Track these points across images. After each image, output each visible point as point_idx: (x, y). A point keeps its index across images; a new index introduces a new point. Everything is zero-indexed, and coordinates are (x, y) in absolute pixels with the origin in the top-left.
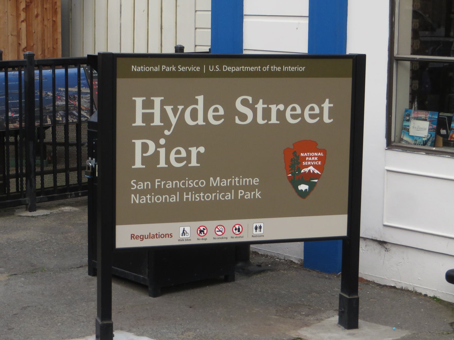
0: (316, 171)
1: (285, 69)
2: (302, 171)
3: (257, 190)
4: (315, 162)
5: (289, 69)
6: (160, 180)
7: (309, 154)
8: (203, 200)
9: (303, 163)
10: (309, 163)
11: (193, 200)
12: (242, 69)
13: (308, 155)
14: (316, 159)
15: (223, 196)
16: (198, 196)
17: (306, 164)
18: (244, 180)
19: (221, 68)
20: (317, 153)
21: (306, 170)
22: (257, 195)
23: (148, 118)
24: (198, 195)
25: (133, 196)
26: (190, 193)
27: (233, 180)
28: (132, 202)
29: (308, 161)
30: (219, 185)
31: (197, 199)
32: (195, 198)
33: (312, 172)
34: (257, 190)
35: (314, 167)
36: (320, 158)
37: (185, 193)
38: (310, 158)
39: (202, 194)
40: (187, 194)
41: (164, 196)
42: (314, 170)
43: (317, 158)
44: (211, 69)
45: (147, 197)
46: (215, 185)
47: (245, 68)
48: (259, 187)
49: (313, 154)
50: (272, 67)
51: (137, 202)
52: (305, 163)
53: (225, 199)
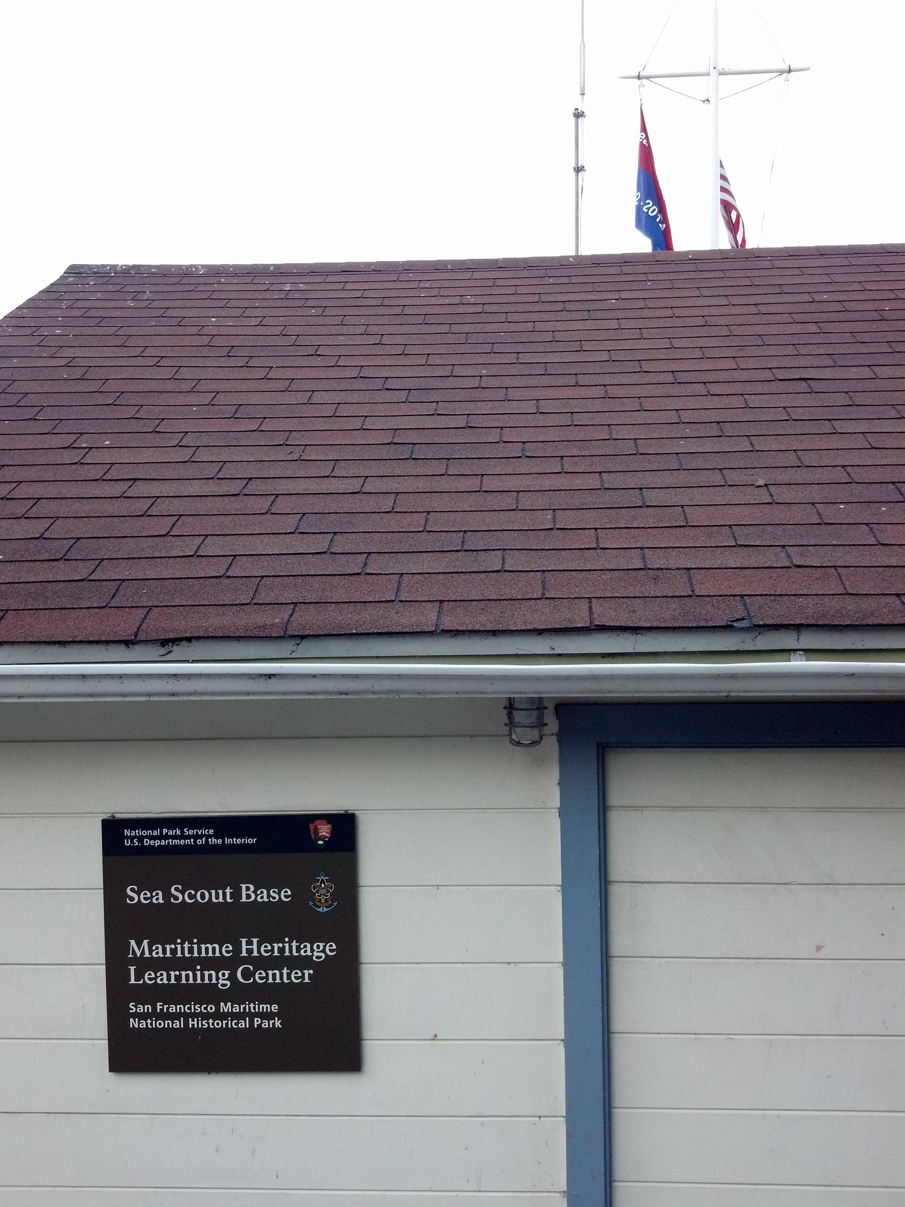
6: (161, 1004)
11: (200, 1027)
12: (169, 842)
18: (261, 1006)
23: (250, 951)
25: (131, 1020)
27: (247, 1006)
30: (230, 1011)
39: (211, 1021)
44: (128, 843)
46: (226, 1011)
48: (278, 1015)
50: (210, 840)
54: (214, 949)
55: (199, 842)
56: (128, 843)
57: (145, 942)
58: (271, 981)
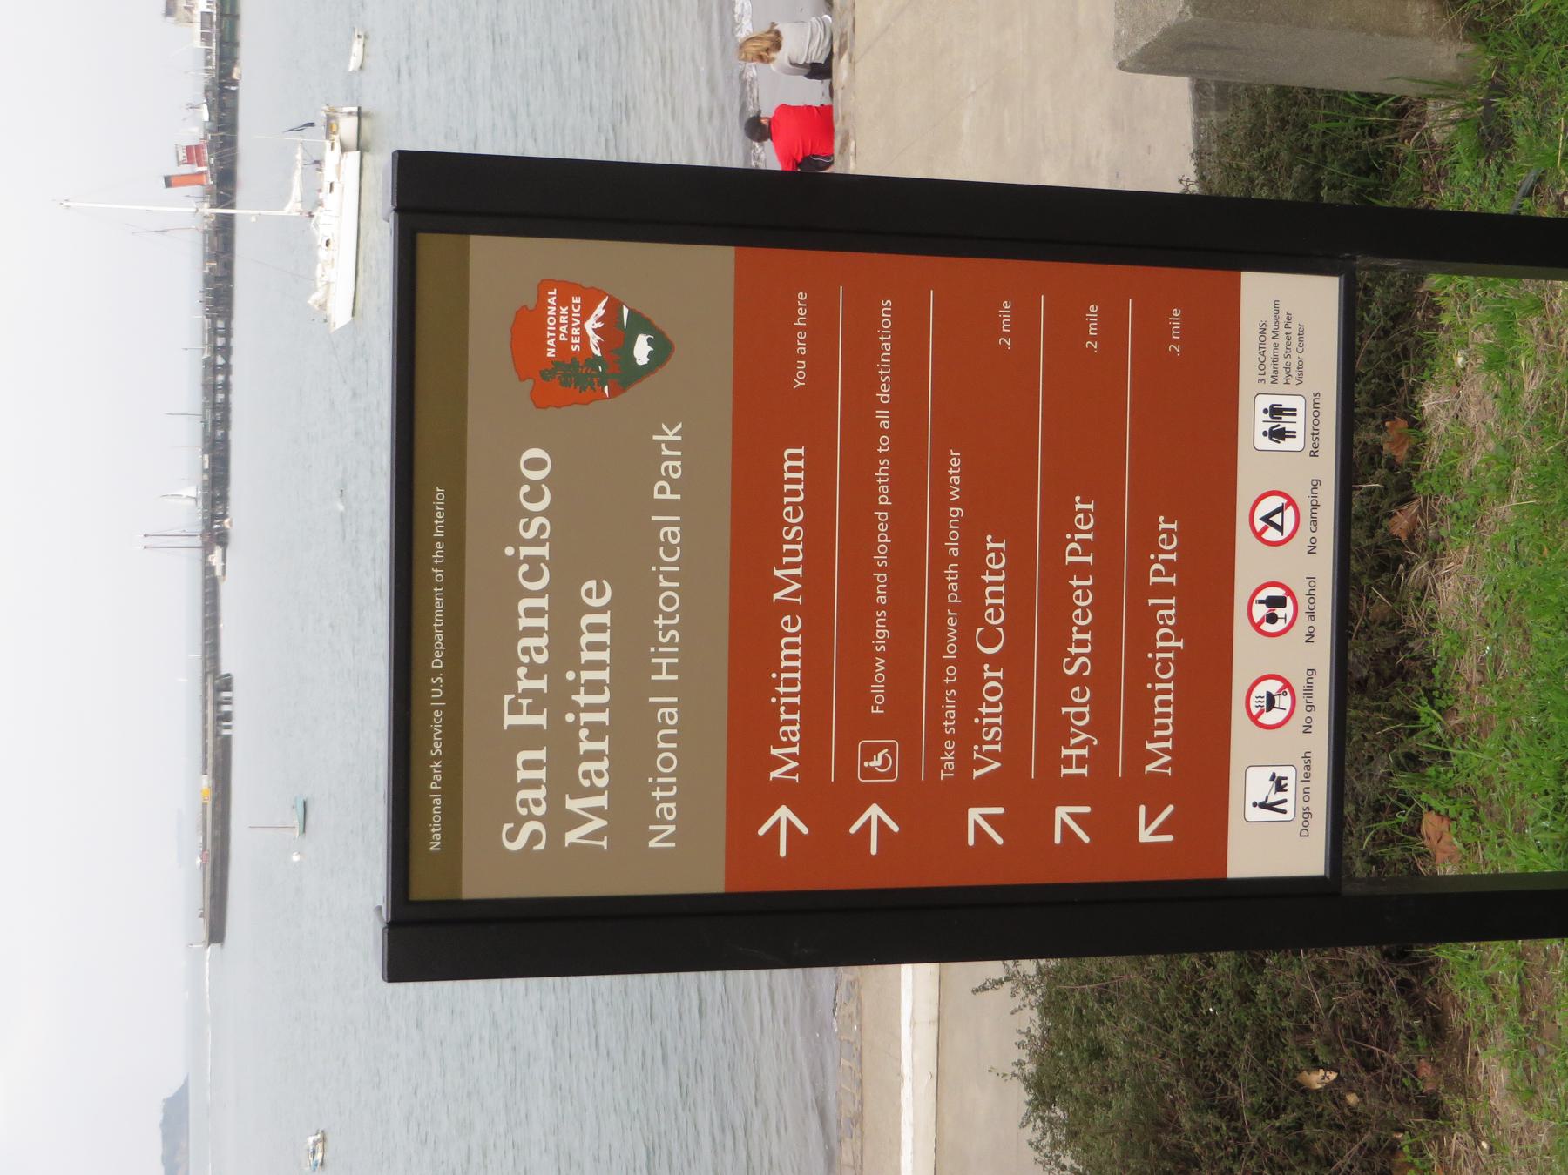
0: (600, 311)
1: (439, 534)
2: (597, 352)
3: (655, 437)
4: (573, 315)
5: (439, 524)
7: (551, 331)
8: (678, 616)
9: (574, 350)
10: (575, 331)
11: (676, 649)
12: (439, 628)
13: (554, 335)
14: (564, 311)
15: (670, 551)
16: (664, 636)
17: (578, 342)
19: (436, 673)
20: (549, 350)
21: (594, 340)
22: (671, 435)
24: (660, 633)
26: (654, 661)
28: (673, 845)
29: (569, 335)
31: (673, 637)
32: (671, 643)
33: (599, 325)
34: (655, 437)
35: (588, 318)
36: (563, 301)
37: (653, 678)
38: (561, 329)
39: (660, 622)
40: (657, 669)
41: (659, 746)
42: (596, 318)
43: (564, 308)
44: (438, 693)
45: (658, 799)
47: (437, 620)
49: (551, 321)
50: (436, 561)
51: (672, 829)
52: (574, 344)
53: (678, 545)
54: (788, 646)
55: (439, 578)
56: (438, 693)
57: (775, 752)
58: (1001, 601)
